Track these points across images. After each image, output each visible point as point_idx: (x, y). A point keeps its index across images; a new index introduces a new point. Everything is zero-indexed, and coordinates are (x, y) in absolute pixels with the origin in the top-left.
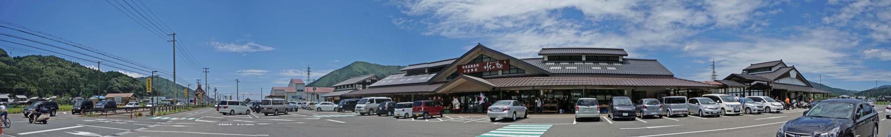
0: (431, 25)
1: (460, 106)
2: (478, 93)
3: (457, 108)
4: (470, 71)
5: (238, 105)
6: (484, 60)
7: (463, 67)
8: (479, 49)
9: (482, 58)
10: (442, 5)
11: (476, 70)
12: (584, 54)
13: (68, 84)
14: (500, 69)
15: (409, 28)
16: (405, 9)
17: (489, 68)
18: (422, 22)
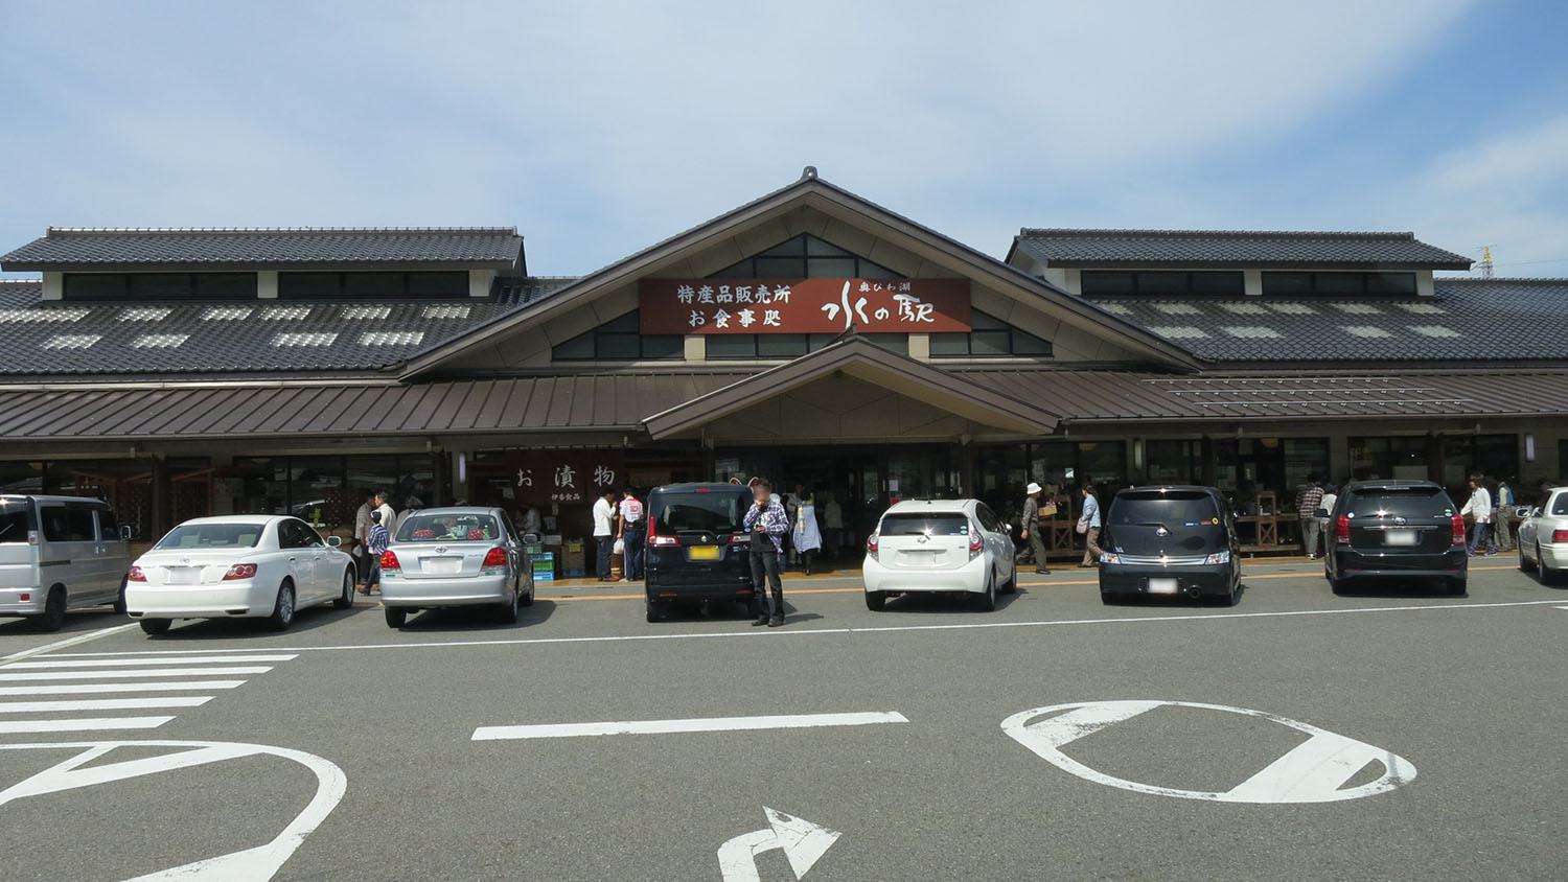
4: (735, 321)
5: (1356, 470)
7: (685, 294)
11: (772, 318)
12: (266, 265)
14: (919, 328)
17: (856, 315)
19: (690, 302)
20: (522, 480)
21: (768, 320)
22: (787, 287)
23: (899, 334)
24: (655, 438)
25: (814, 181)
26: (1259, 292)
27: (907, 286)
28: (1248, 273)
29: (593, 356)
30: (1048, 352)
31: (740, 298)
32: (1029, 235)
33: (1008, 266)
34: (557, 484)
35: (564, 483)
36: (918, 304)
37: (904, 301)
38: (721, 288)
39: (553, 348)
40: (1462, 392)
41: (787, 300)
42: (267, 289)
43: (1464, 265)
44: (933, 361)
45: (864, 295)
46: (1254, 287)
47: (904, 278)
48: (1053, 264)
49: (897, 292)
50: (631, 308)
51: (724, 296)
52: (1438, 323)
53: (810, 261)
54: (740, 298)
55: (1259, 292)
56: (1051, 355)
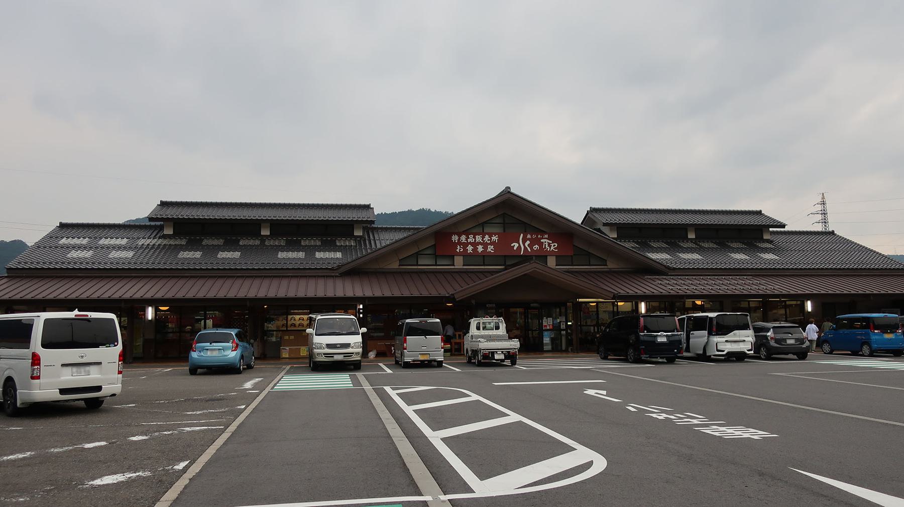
4: (475, 249)
7: (455, 238)
11: (490, 248)
14: (552, 253)
19: (456, 242)
21: (489, 250)
23: (542, 257)
24: (457, 300)
25: (509, 192)
27: (546, 236)
29: (434, 264)
30: (605, 264)
31: (477, 240)
32: (593, 210)
33: (582, 225)
37: (545, 242)
38: (470, 236)
39: (400, 260)
40: (769, 283)
42: (265, 232)
43: (783, 226)
44: (557, 267)
45: (529, 239)
47: (545, 233)
48: (605, 225)
49: (543, 238)
50: (433, 244)
51: (471, 239)
52: (771, 252)
54: (477, 240)
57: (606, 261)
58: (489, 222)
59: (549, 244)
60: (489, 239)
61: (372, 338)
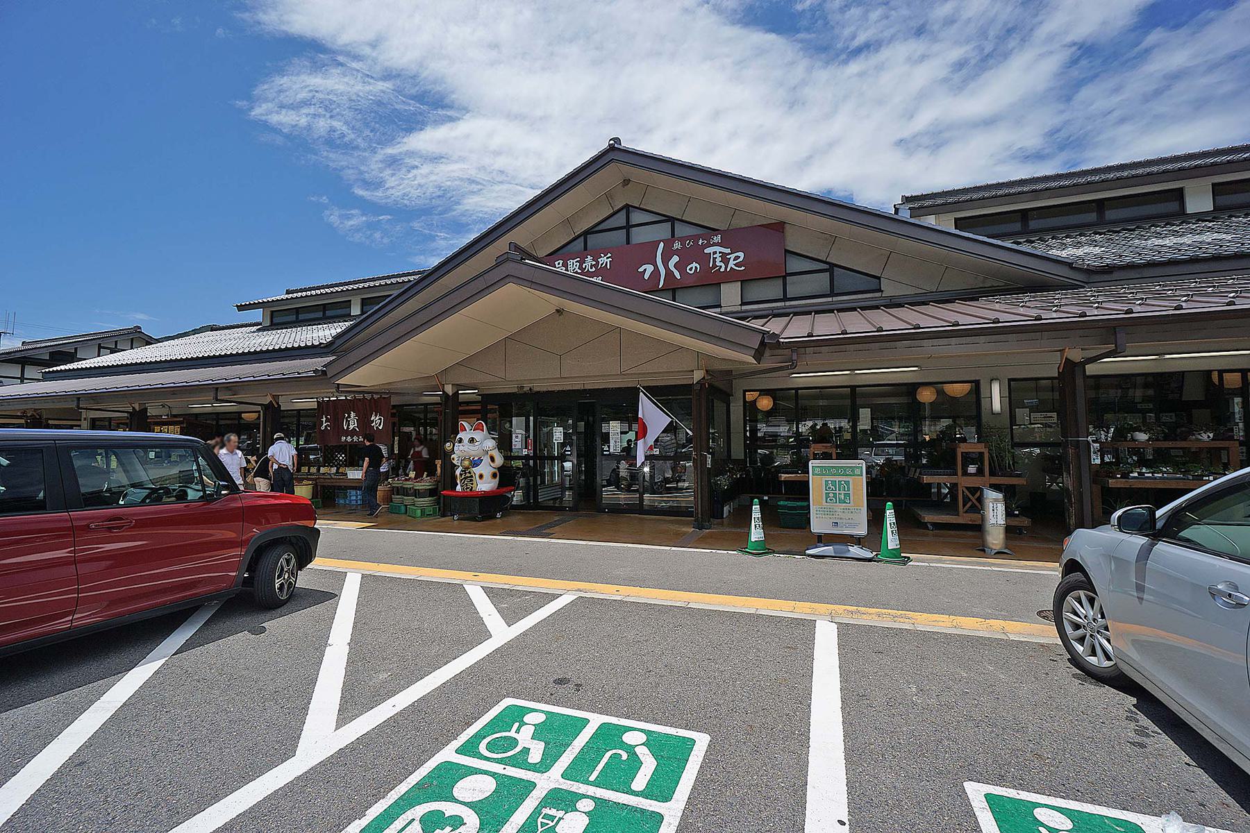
0: (445, 239)
1: (505, 476)
2: (630, 396)
3: (486, 484)
6: (641, 236)
8: (610, 176)
9: (628, 227)
10: (479, 187)
13: (872, 439)
14: (730, 277)
15: (377, 235)
16: (367, 184)
18: (416, 225)
20: (324, 425)
22: (609, 255)
26: (1208, 206)
28: (1189, 185)
34: (345, 428)
35: (351, 427)
36: (729, 254)
37: (715, 253)
41: (646, 277)
44: (744, 308)
45: (677, 252)
46: (1199, 200)
53: (780, 282)
55: (1208, 206)
56: (880, 290)
57: (879, 278)
58: (596, 229)
59: (724, 255)
60: (594, 263)
61: (131, 427)
